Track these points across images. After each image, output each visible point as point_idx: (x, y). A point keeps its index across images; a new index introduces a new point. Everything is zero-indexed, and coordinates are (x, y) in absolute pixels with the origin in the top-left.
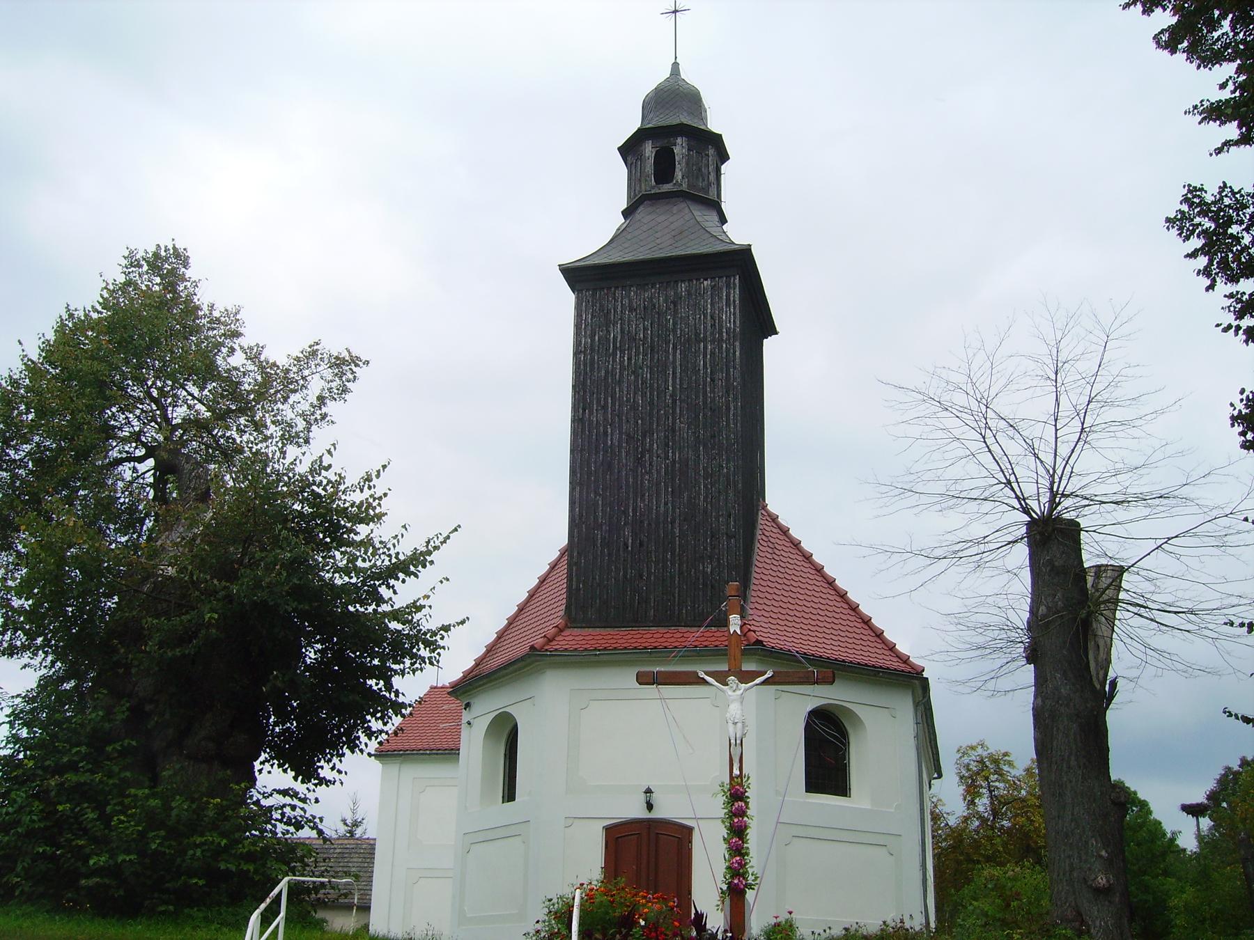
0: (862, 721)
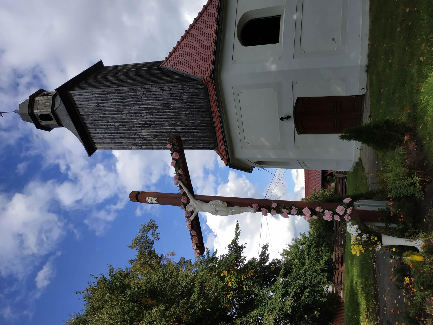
0: (245, 14)
